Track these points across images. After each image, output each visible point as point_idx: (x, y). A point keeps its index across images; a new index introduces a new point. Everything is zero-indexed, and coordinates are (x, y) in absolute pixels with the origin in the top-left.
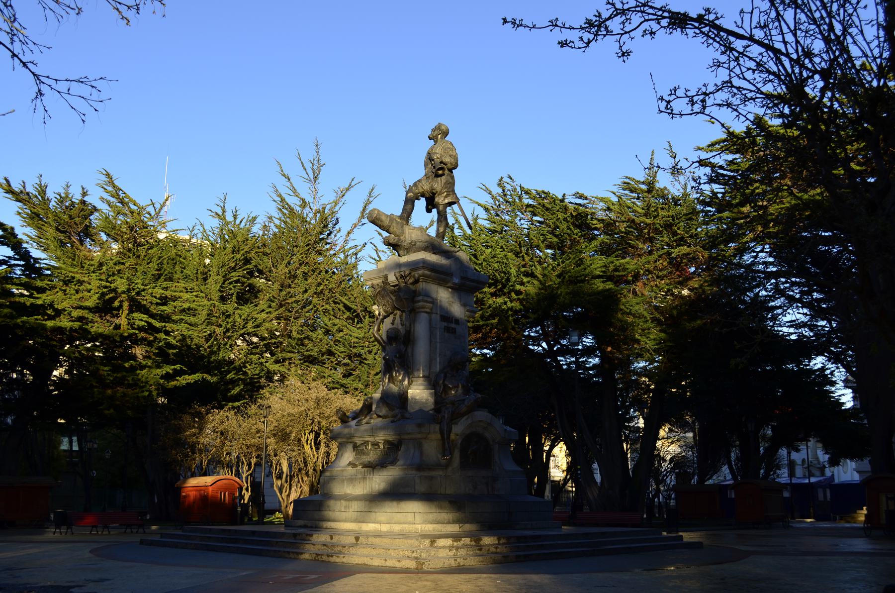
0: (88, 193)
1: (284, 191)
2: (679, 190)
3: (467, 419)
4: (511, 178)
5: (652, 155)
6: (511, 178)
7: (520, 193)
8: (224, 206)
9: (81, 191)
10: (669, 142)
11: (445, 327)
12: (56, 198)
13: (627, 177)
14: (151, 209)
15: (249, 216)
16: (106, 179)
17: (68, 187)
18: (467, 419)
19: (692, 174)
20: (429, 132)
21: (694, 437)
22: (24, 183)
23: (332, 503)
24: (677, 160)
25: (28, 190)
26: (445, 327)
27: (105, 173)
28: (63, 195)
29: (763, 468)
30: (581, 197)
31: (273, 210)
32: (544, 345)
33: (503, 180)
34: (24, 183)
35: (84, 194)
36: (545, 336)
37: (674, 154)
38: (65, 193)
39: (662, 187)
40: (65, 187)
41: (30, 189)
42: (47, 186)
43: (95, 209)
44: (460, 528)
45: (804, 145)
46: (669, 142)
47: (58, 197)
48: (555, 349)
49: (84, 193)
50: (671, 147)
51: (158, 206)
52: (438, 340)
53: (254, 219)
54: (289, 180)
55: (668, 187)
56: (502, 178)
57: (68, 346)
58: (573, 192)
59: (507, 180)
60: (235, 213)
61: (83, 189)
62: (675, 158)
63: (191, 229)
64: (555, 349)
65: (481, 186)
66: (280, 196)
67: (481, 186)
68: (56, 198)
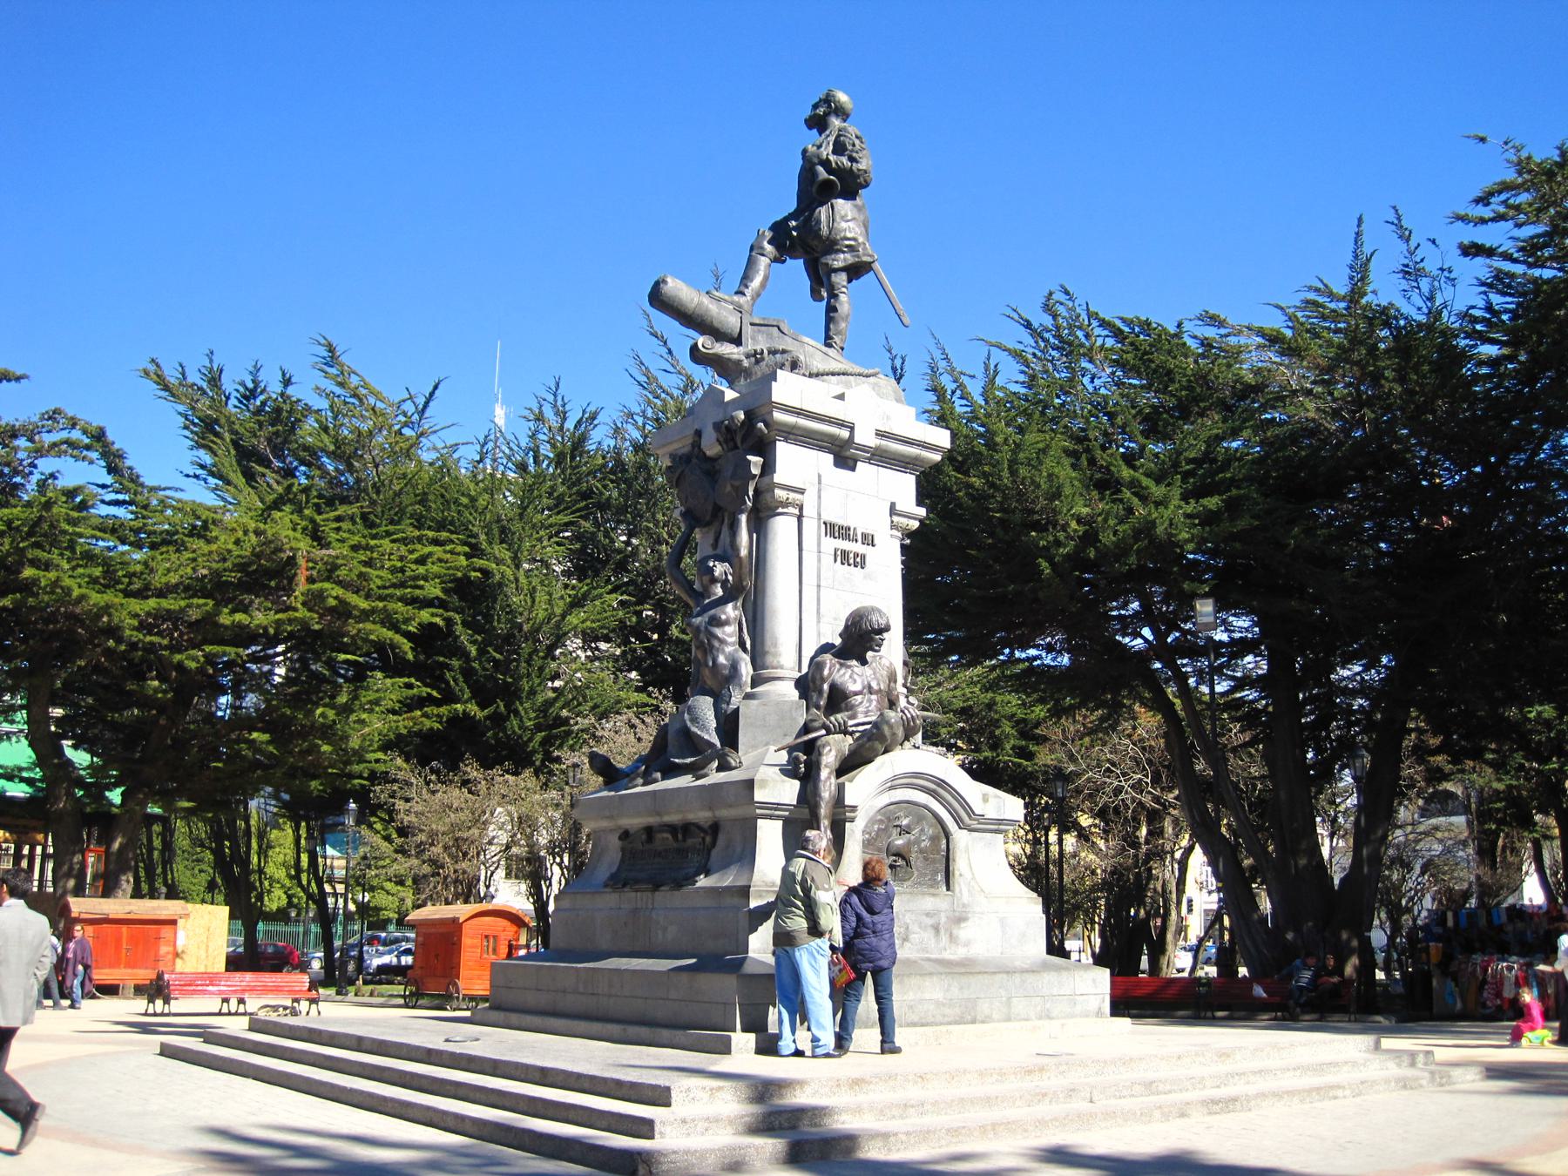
0: (293, 380)
1: (656, 365)
2: (1419, 309)
4: (1067, 293)
5: (1359, 226)
6: (1067, 293)
7: (1086, 322)
10: (1394, 208)
12: (237, 391)
13: (1310, 288)
14: (409, 407)
15: (584, 412)
16: (326, 354)
19: (1446, 273)
20: (807, 112)
21: (1469, 823)
22: (181, 365)
24: (1413, 244)
25: (190, 380)
27: (323, 341)
28: (250, 385)
30: (1214, 320)
31: (633, 399)
32: (1146, 632)
33: (1054, 296)
34: (181, 365)
35: (287, 382)
36: (1147, 616)
37: (1407, 233)
38: (253, 381)
39: (1384, 303)
41: (194, 378)
42: (221, 371)
43: (308, 408)
45: (1380, 679)
46: (1394, 208)
47: (242, 389)
48: (1169, 640)
50: (1399, 219)
51: (421, 401)
53: (593, 417)
54: (665, 343)
55: (1397, 305)
56: (1051, 294)
58: (1198, 311)
59: (1059, 296)
61: (284, 374)
62: (1408, 240)
63: (482, 440)
64: (1169, 640)
65: (1009, 312)
66: (647, 374)
67: (1009, 312)
68: (237, 391)
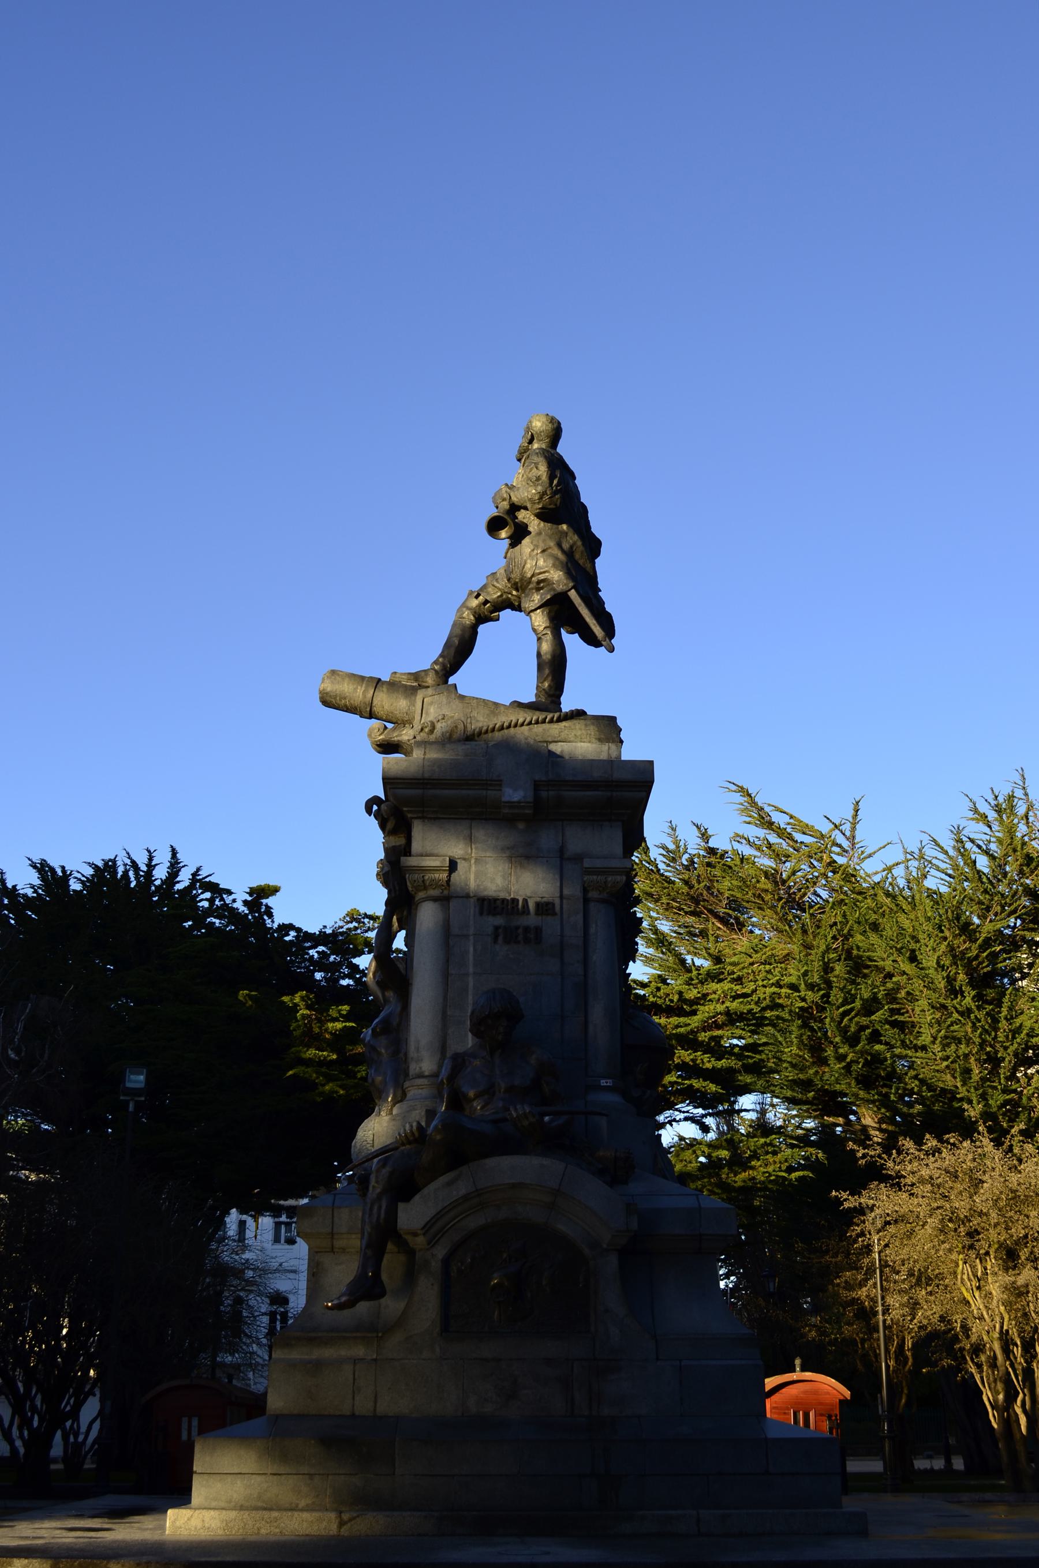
0: (710, 832)
3: (449, 1184)
8: (1026, 794)
9: (695, 832)
11: (496, 928)
16: (742, 800)
17: (674, 829)
18: (449, 1184)
23: (357, 1413)
26: (496, 928)
27: (734, 788)
29: (66, 1327)
35: (705, 836)
40: (670, 831)
44: (342, 1524)
49: (703, 835)
52: (471, 970)
57: (812, 1139)
60: (993, 803)
61: (698, 827)
